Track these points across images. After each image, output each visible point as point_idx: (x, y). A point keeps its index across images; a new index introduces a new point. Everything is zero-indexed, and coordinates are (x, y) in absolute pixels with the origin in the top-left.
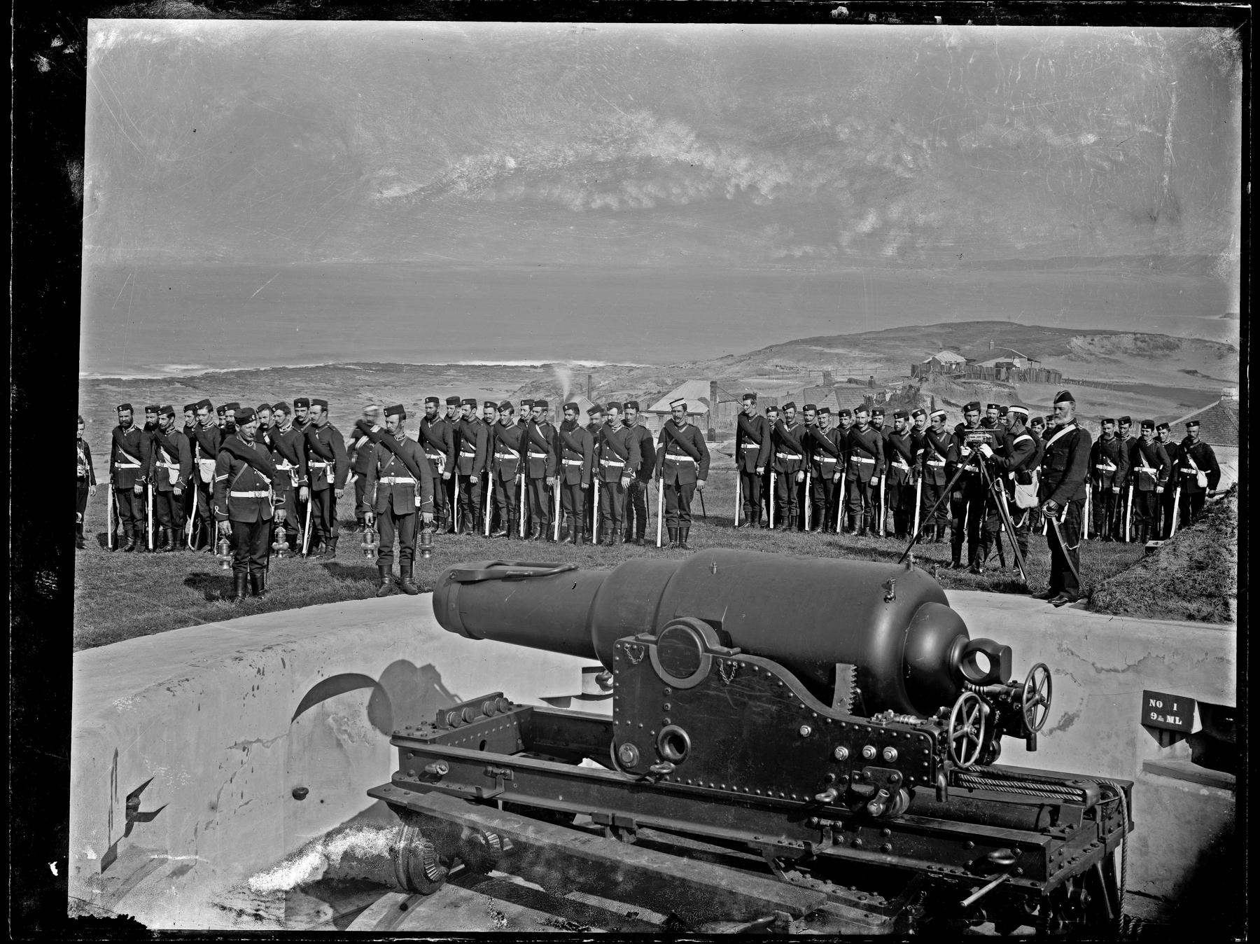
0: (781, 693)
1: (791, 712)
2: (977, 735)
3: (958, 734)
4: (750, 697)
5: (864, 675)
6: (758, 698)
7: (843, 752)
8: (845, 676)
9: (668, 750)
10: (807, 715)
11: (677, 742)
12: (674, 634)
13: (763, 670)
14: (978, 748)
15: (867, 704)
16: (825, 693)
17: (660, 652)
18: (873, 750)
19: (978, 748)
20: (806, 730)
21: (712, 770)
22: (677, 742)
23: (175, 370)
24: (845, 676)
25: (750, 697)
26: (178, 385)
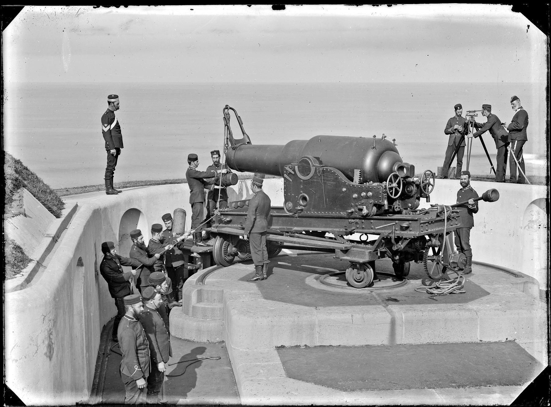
0: (336, 178)
1: (339, 184)
2: (399, 187)
3: (390, 186)
4: (327, 180)
5: (362, 173)
6: (330, 181)
7: (355, 196)
8: (357, 173)
9: (301, 202)
10: (344, 185)
11: (304, 199)
12: (303, 161)
13: (331, 170)
14: (400, 193)
15: (364, 180)
16: (352, 179)
17: (298, 168)
18: (365, 194)
19: (400, 193)
20: (344, 189)
21: (315, 208)
22: (304, 199)
23: (296, 228)
24: (357, 173)
25: (327, 180)
26: (403, 349)
